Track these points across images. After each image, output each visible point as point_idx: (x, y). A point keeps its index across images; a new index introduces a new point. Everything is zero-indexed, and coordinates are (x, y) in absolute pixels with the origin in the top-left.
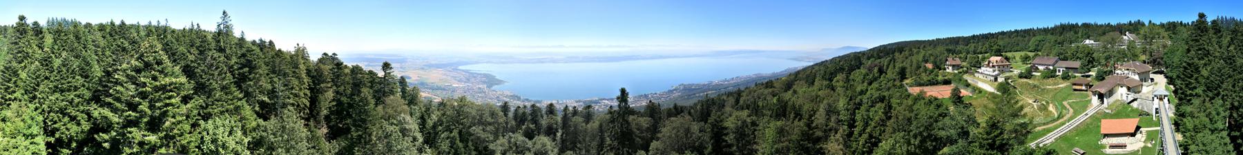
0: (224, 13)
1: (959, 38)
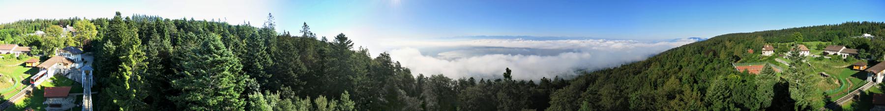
0: (305, 23)
1: (773, 31)
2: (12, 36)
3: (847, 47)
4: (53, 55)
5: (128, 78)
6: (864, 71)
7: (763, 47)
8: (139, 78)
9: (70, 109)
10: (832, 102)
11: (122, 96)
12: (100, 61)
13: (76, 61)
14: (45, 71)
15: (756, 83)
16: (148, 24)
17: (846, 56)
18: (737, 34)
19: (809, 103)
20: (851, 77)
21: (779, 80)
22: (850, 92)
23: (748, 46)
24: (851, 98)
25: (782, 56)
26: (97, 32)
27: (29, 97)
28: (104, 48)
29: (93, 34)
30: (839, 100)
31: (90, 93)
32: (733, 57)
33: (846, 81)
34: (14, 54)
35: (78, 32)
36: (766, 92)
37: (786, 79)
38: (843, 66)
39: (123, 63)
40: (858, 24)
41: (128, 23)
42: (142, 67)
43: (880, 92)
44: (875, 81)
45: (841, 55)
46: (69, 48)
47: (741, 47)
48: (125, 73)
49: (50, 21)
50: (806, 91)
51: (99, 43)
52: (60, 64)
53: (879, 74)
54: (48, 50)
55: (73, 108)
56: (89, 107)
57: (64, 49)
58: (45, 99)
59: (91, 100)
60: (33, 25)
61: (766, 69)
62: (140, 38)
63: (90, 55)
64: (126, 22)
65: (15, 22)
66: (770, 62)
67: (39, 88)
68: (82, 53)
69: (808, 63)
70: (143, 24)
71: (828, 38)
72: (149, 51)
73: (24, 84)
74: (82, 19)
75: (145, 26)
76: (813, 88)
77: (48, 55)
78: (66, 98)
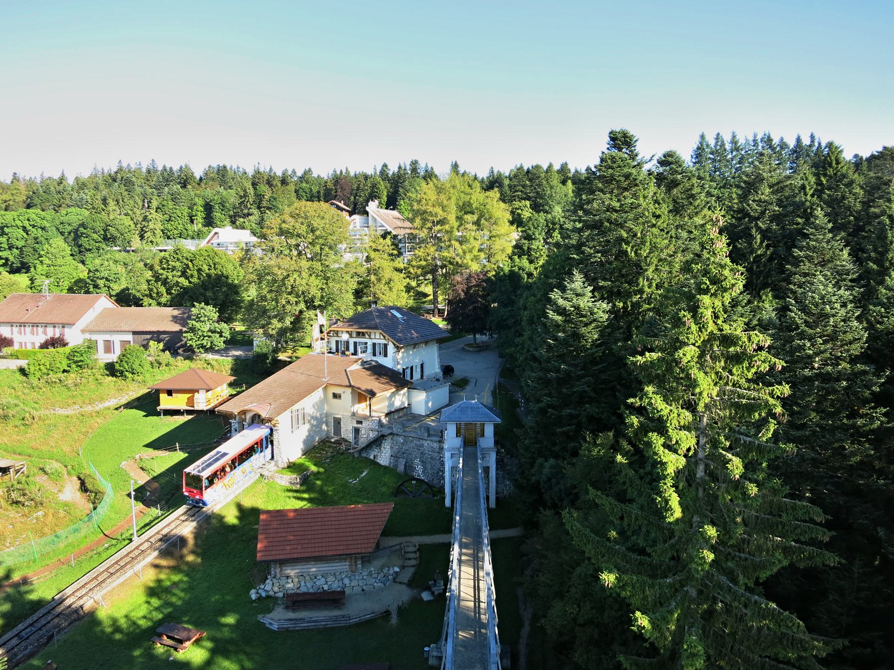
2: (80, 251)
4: (301, 352)
5: (673, 462)
8: (736, 466)
9: (387, 613)
11: (642, 552)
12: (530, 379)
13: (417, 375)
14: (259, 433)
16: (777, 187)
26: (515, 235)
27: (175, 569)
28: (551, 314)
29: (498, 245)
31: (486, 533)
34: (91, 346)
35: (423, 234)
38: (102, 400)
39: (650, 389)
41: (674, 184)
42: (750, 408)
46: (382, 313)
48: (657, 440)
49: (284, 182)
51: (529, 287)
52: (336, 396)
54: (276, 324)
55: (400, 609)
56: (477, 600)
57: (356, 320)
58: (263, 571)
59: (488, 566)
60: (197, 196)
62: (736, 256)
63: (481, 348)
64: (660, 178)
65: (93, 177)
67: (231, 518)
68: (442, 341)
70: (750, 186)
72: (792, 327)
73: (148, 503)
74: (443, 171)
75: (765, 192)
77: (276, 351)
78: (366, 559)
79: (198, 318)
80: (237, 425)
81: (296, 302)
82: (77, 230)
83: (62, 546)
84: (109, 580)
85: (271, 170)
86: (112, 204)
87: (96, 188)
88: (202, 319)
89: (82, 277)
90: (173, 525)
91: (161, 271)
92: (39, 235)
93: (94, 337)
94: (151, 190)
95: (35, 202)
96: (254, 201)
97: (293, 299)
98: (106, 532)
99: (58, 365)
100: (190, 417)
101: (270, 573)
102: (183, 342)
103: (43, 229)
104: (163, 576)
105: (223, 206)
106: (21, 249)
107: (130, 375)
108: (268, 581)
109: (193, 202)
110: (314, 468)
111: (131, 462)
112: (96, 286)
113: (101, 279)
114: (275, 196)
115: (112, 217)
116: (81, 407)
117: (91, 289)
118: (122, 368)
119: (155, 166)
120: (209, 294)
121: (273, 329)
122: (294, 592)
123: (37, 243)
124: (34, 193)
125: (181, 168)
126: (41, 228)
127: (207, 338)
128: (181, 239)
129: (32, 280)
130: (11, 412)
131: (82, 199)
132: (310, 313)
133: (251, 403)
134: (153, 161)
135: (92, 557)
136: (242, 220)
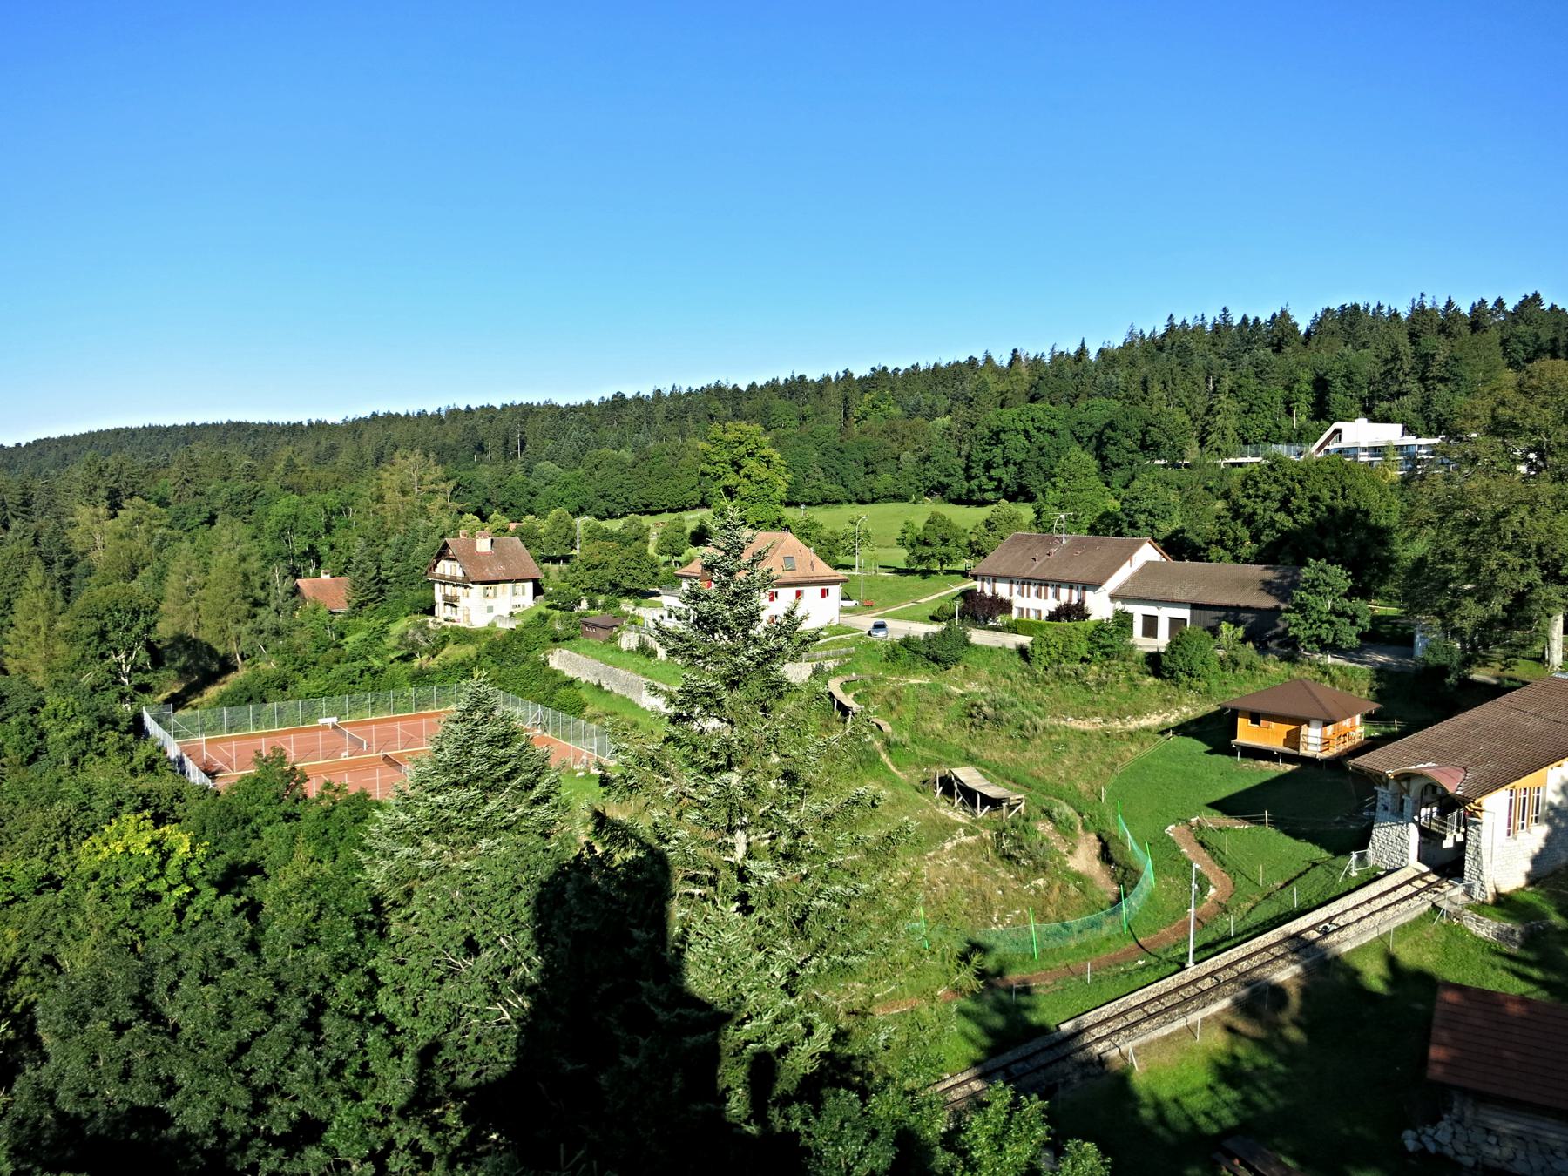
1: (527, 411)
3: (1176, 547)
6: (1336, 763)
7: (443, 553)
10: (1042, 1030)
15: (377, 875)
17: (1163, 628)
18: (192, 433)
19: (841, 1036)
20: (1214, 820)
21: (582, 833)
22: (1208, 949)
23: (299, 544)
24: (1214, 1009)
25: (610, 631)
27: (1263, 1044)
30: (1106, 1011)
32: (157, 657)
33: (1166, 853)
36: (472, 948)
37: (643, 825)
38: (1138, 713)
40: (1280, 333)
43: (1503, 983)
44: (1449, 865)
45: (1124, 621)
47: (222, 560)
50: (818, 932)
53: (1495, 806)
61: (465, 747)
66: (502, 683)
69: (834, 686)
71: (1005, 474)
76: (872, 899)
79: (1313, 587)
80: (1389, 799)
81: (1522, 566)
82: (1102, 433)
83: (1073, 943)
84: (1144, 1025)
85: (1449, 304)
86: (1156, 391)
87: (1132, 364)
88: (1321, 589)
89: (1111, 509)
90: (1256, 961)
91: (1243, 501)
92: (1046, 443)
93: (1130, 608)
94: (1219, 362)
95: (1042, 394)
96: (1413, 368)
97: (1514, 560)
98: (1140, 940)
99: (1075, 649)
100: (1290, 767)
101: (1449, 1110)
102: (1279, 630)
103: (1053, 433)
104: (1240, 1051)
105: (1350, 381)
106: (1020, 465)
107: (1186, 678)
108: (1442, 1124)
109: (1293, 377)
110: (1556, 919)
111: (1183, 828)
112: (1133, 525)
113: (1141, 513)
114: (1458, 354)
115: (1155, 411)
116: (1105, 721)
117: (1125, 530)
118: (1173, 665)
119: (1229, 319)
120: (1331, 544)
121: (1463, 618)
122: (1497, 1165)
123: (1043, 455)
124: (1041, 378)
125: (1274, 316)
126: (1048, 431)
127: (1326, 625)
128: (1268, 444)
129: (1039, 513)
130: (1006, 715)
131: (1111, 383)
132: (1550, 589)
133: (1424, 761)
134: (1225, 310)
135: (1117, 976)
136: (1385, 404)
